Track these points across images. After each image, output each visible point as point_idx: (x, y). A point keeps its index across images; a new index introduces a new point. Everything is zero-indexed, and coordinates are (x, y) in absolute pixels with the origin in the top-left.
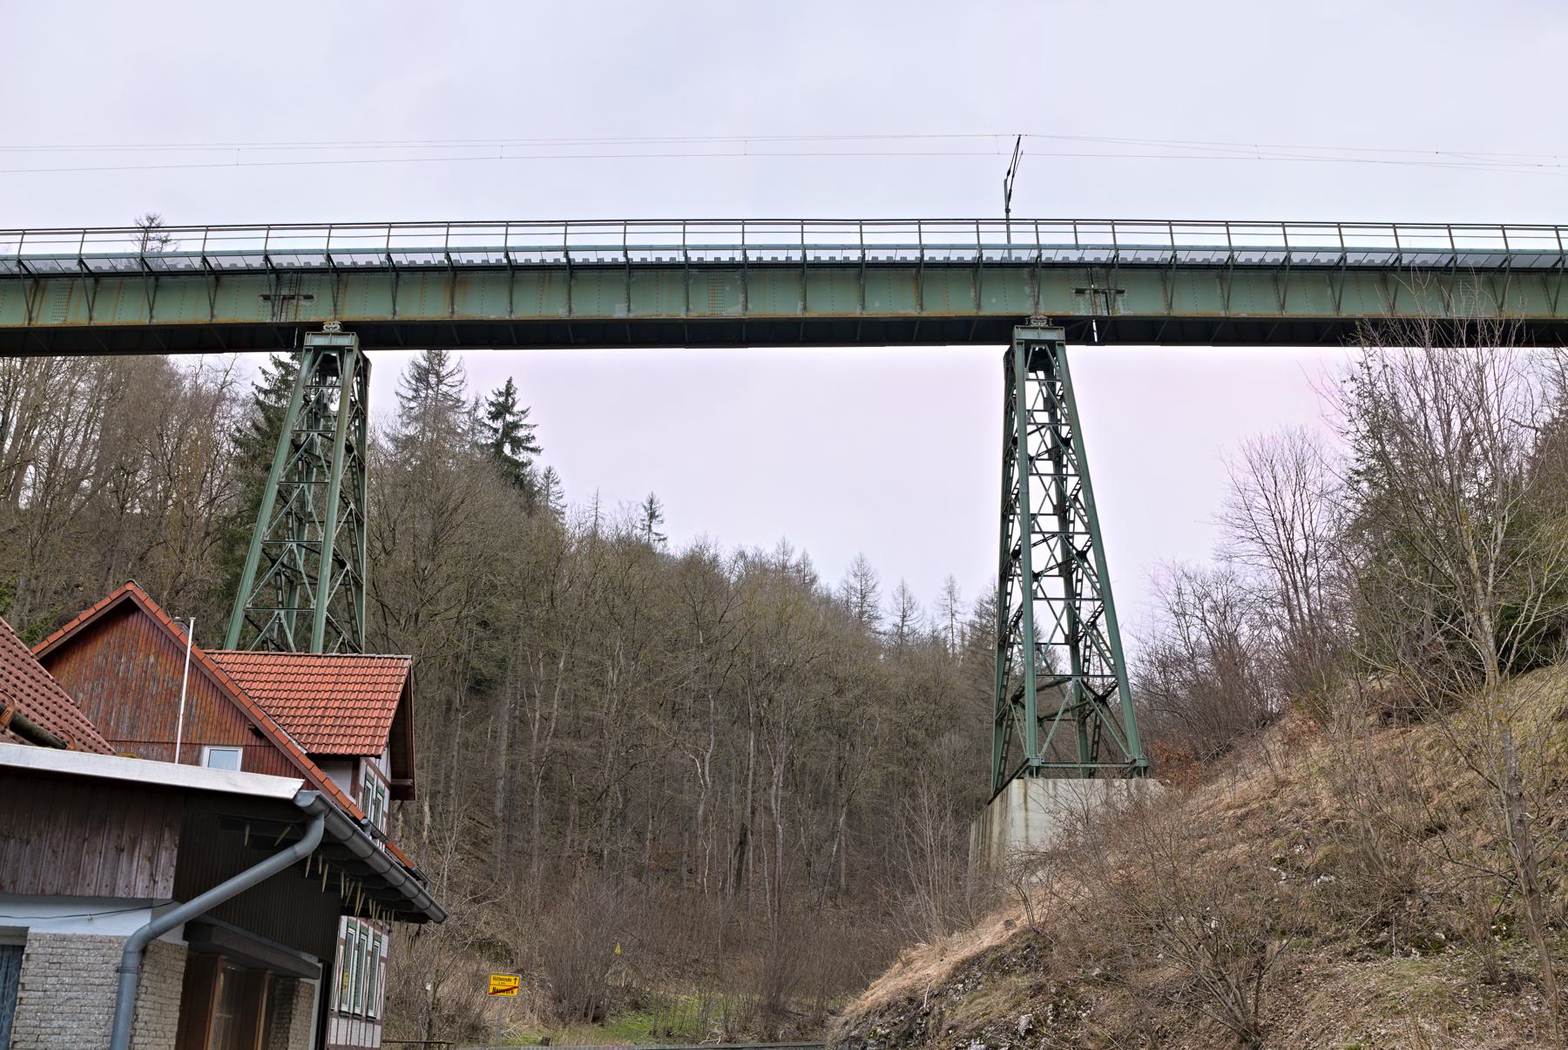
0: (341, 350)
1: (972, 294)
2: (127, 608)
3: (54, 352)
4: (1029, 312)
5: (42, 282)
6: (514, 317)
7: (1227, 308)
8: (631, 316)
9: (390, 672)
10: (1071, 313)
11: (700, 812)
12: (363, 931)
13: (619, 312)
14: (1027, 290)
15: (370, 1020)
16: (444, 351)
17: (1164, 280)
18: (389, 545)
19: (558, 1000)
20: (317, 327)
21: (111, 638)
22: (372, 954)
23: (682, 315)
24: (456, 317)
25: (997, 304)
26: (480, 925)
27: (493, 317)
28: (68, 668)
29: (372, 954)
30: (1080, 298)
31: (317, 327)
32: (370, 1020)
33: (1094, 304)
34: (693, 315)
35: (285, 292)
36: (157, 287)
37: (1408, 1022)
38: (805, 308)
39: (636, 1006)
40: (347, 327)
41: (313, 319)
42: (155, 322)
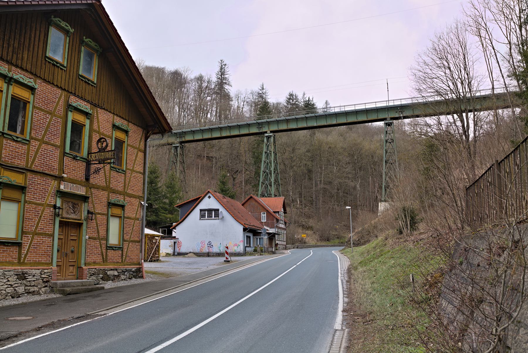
2: (251, 197)
4: (387, 117)
6: (298, 127)
8: (317, 125)
11: (358, 196)
12: (282, 231)
13: (315, 125)
14: (210, 132)
15: (284, 241)
17: (240, 127)
18: (284, 152)
19: (321, 237)
20: (266, 132)
21: (250, 200)
22: (283, 233)
23: (326, 124)
24: (288, 128)
25: (381, 116)
26: (309, 223)
28: (245, 205)
29: (283, 233)
30: (397, 113)
31: (266, 132)
32: (284, 241)
33: (399, 114)
35: (260, 127)
38: (347, 121)
39: (338, 238)
40: (271, 132)
41: (265, 131)
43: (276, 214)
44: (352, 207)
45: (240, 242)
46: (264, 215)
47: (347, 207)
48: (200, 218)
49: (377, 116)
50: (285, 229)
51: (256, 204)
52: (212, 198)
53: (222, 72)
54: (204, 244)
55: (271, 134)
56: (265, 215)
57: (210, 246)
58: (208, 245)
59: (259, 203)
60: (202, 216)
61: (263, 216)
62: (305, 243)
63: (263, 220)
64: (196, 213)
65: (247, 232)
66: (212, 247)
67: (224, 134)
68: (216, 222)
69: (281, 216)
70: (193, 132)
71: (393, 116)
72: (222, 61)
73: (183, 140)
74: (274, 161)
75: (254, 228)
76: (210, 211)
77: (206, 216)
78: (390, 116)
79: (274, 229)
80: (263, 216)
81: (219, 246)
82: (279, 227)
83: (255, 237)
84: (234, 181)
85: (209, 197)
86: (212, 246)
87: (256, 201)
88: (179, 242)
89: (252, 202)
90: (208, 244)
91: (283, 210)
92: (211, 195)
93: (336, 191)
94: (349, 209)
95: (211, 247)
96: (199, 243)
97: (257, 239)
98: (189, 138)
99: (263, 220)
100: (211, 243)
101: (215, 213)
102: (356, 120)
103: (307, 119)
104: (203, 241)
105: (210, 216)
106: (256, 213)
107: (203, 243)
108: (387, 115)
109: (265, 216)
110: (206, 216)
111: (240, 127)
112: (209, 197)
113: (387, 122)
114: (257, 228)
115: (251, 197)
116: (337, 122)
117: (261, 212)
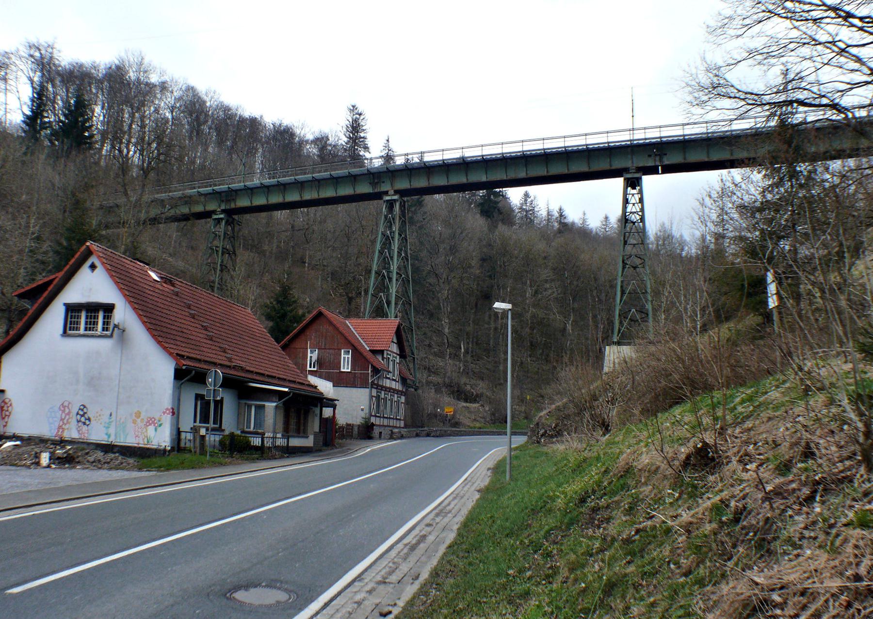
0: (395, 200)
1: (609, 160)
3: (732, 167)
5: (270, 189)
7: (708, 157)
9: (392, 323)
10: (646, 165)
14: (629, 156)
16: (504, 189)
20: (386, 193)
25: (618, 164)
27: (442, 184)
31: (386, 193)
33: (655, 160)
34: (509, 178)
36: (252, 193)
37: (828, 574)
38: (547, 172)
40: (396, 192)
42: (338, 195)
43: (378, 357)
44: (513, 305)
45: (164, 413)
46: (346, 356)
47: (497, 305)
48: (65, 332)
49: (610, 162)
50: (402, 392)
51: (331, 328)
52: (100, 270)
53: (355, 128)
54: (69, 414)
55: (395, 197)
56: (350, 356)
57: (83, 419)
58: (79, 417)
59: (336, 328)
60: (69, 328)
61: (344, 358)
62: (457, 424)
63: (344, 368)
64: (55, 316)
65: (188, 380)
66: (87, 422)
67: (308, 196)
68: (104, 345)
69: (391, 363)
70: (249, 191)
71: (641, 165)
72: (353, 106)
73: (233, 206)
74: (399, 253)
75: (243, 375)
76: (93, 309)
77: (82, 326)
78: (635, 165)
79: (367, 390)
80: (344, 358)
81: (108, 421)
82: (382, 387)
83: (243, 402)
84: (350, 303)
85: (93, 267)
86: (89, 419)
87: (331, 323)
88: (7, 401)
89: (323, 327)
90: (78, 414)
91: (395, 348)
92: (97, 263)
93: (528, 330)
94: (505, 312)
95: (84, 423)
96: (56, 409)
97: (250, 407)
98: (243, 202)
99: (344, 368)
100: (85, 410)
101: (87, 318)
102: (566, 171)
103: (355, 178)
104: (66, 404)
105: (91, 325)
106: (331, 351)
107: (67, 411)
108: (630, 162)
109: (348, 358)
110: (82, 326)
111: (252, 194)
112: (93, 267)
113: (629, 176)
114: (250, 376)
115: (320, 314)
116: (527, 173)
117: (340, 350)
